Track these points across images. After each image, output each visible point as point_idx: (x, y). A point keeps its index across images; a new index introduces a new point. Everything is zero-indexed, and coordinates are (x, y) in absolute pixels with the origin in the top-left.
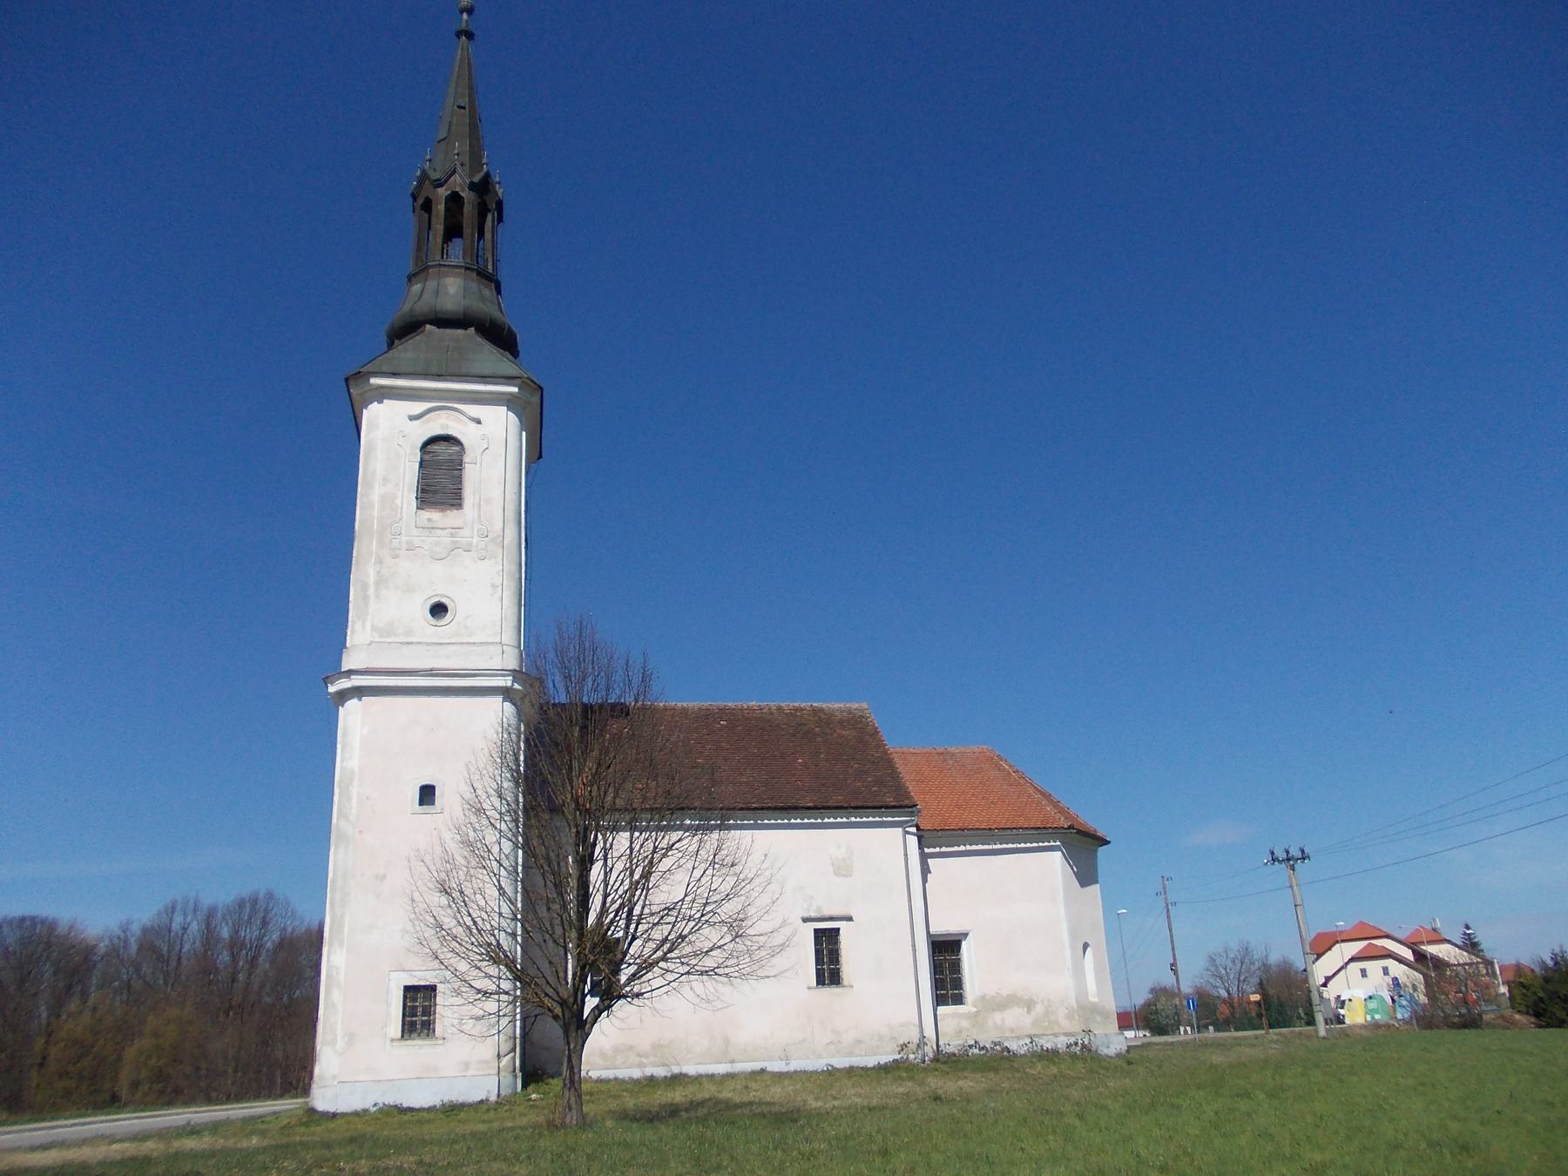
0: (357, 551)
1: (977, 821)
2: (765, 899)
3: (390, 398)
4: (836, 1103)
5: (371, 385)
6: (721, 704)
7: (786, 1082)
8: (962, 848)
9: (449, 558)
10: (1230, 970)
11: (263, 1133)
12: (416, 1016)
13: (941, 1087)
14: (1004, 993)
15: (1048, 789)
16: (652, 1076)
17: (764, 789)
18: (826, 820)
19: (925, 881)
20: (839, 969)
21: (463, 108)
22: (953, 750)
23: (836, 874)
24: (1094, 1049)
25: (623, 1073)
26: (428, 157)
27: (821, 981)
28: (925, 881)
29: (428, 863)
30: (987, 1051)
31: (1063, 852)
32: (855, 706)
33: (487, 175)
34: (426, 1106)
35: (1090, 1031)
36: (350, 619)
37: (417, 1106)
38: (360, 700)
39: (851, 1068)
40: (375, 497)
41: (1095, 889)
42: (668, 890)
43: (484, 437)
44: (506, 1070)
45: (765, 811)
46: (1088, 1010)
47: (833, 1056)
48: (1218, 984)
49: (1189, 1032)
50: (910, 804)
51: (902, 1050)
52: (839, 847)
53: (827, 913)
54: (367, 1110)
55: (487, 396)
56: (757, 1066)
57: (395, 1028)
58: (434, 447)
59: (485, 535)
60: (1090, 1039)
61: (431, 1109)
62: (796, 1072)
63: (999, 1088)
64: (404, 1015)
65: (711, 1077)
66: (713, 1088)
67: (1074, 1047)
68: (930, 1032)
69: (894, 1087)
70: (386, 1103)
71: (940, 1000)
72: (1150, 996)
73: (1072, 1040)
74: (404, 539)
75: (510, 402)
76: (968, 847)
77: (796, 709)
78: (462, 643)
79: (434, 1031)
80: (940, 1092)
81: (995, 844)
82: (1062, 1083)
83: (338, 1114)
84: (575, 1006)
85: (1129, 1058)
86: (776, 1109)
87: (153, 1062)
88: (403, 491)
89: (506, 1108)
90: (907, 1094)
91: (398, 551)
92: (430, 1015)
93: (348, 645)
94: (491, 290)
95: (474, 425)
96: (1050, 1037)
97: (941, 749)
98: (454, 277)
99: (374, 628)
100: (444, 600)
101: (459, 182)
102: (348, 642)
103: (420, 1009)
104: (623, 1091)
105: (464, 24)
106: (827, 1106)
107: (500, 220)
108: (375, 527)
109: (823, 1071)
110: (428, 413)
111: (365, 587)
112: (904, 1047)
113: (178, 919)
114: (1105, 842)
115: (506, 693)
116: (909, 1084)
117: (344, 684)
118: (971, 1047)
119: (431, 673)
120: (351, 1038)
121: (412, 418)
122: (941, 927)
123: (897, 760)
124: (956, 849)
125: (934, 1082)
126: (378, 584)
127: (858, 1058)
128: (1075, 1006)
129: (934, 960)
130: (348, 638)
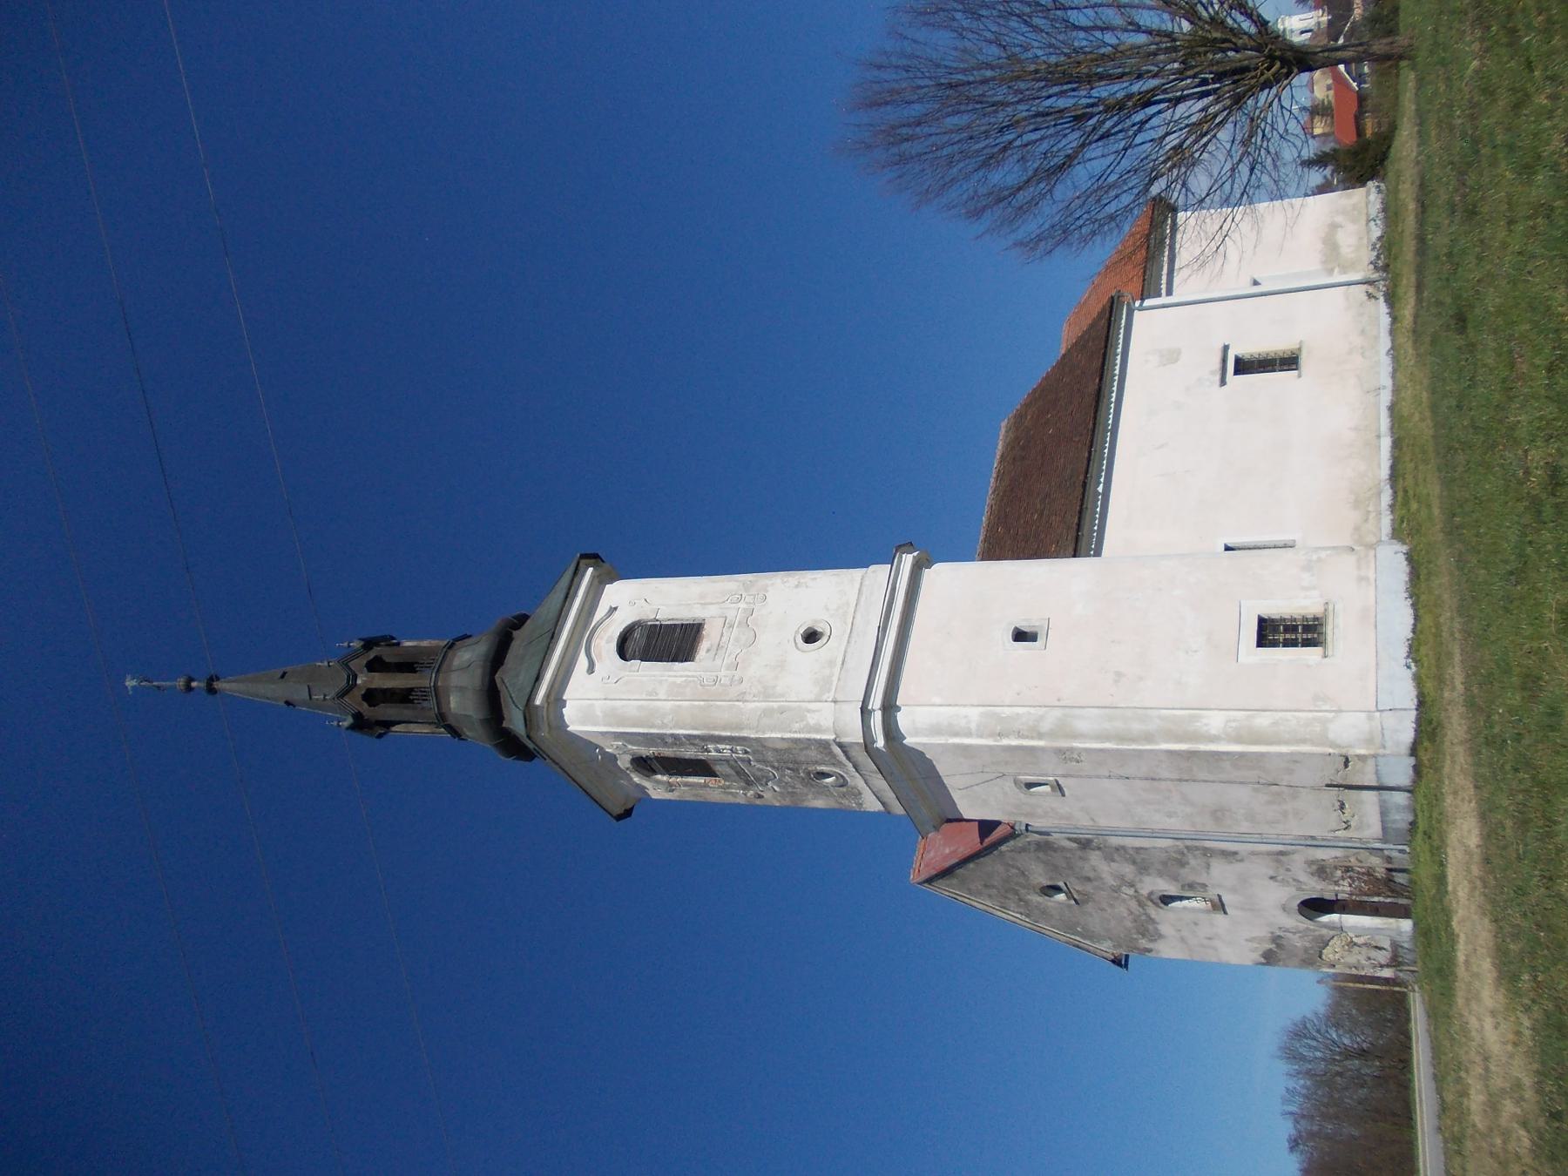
0: (724, 729)
18: (1117, 372)
23: (1177, 360)
34: (1412, 622)
38: (898, 709)
55: (590, 598)
58: (630, 647)
70: (1405, 655)
95: (616, 614)
103: (1288, 636)
119: (883, 629)
121: (591, 669)
127: (1382, 330)
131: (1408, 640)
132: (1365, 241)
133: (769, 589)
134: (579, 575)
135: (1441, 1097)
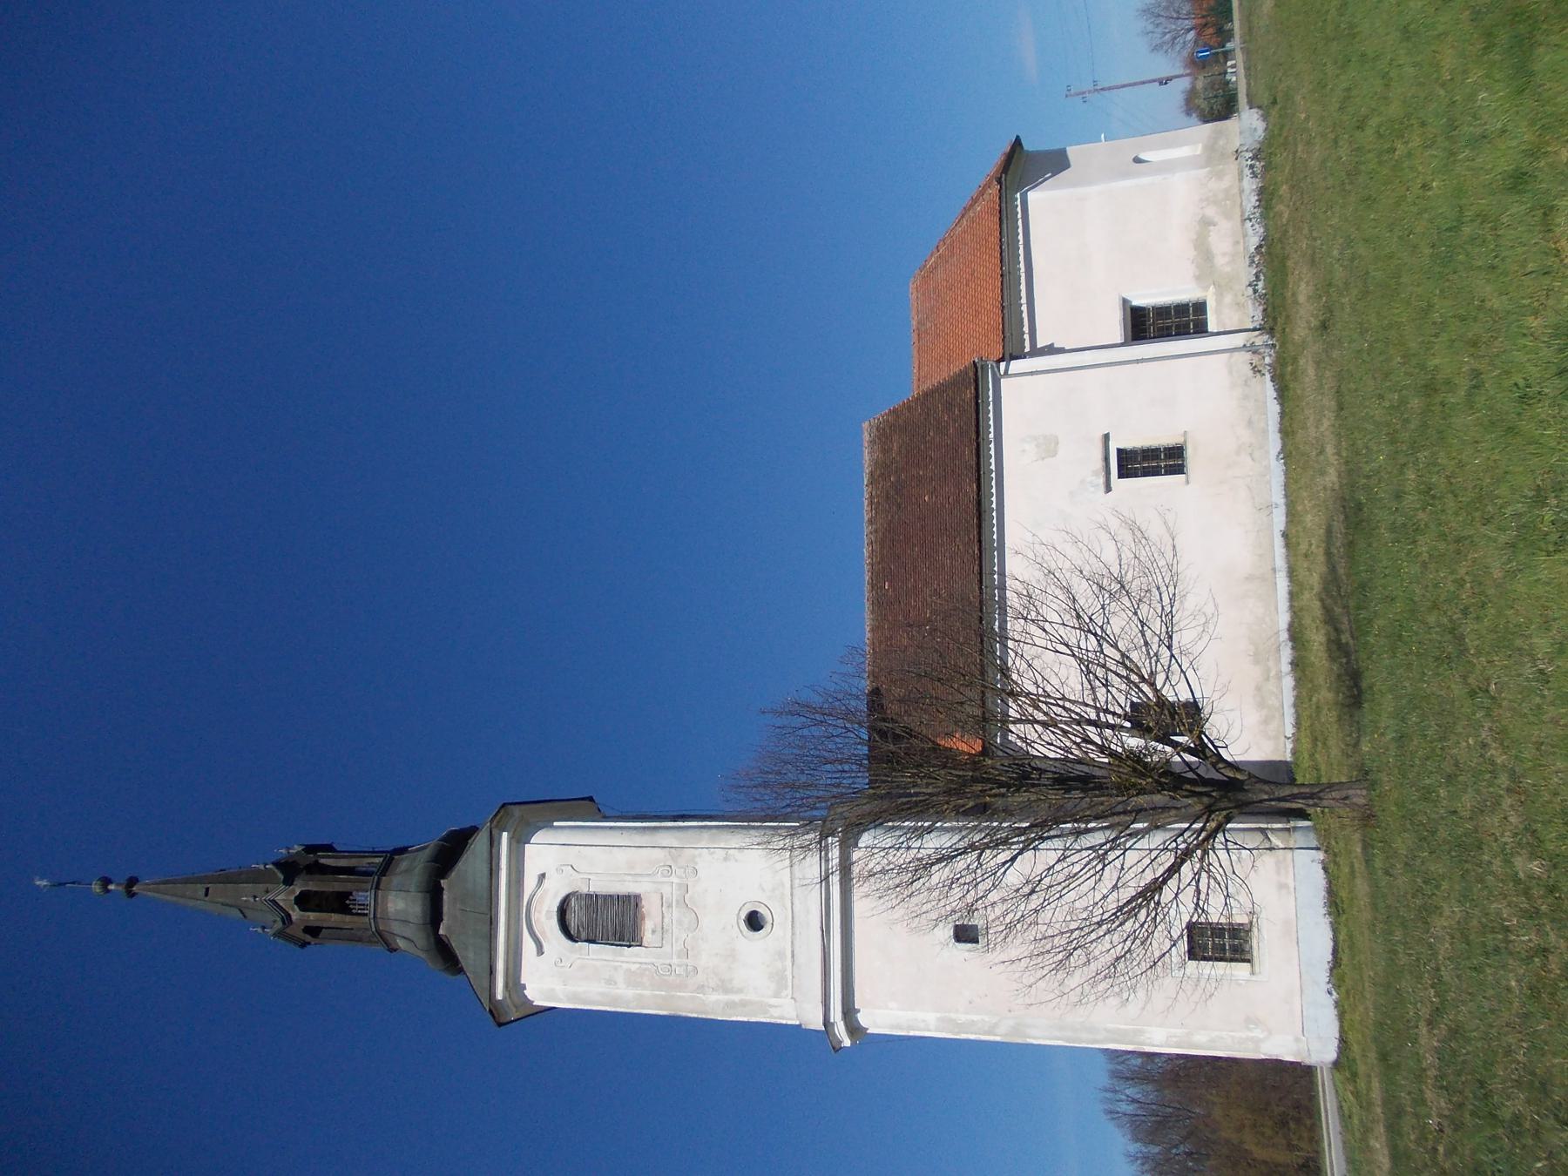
1: (993, 291)
2: (1071, 551)
3: (519, 977)
4: (1330, 450)
5: (504, 998)
6: (867, 587)
7: (1299, 508)
8: (1024, 308)
9: (695, 909)
10: (1166, 28)
11: (1367, 1130)
12: (1224, 944)
13: (1308, 322)
14: (1192, 253)
15: (959, 211)
16: (1291, 664)
17: (958, 540)
18: (993, 467)
19: (1062, 351)
20: (1165, 448)
21: (207, 889)
22: (914, 323)
23: (1054, 454)
24: (1258, 146)
25: (1288, 697)
26: (259, 930)
27: (1179, 469)
28: (1062, 351)
29: (1032, 980)
30: (1260, 272)
31: (1028, 190)
32: (866, 437)
33: (276, 864)
35: (1237, 151)
36: (768, 1020)
37: (1331, 944)
38: (859, 1011)
39: (1281, 431)
40: (630, 993)
41: (1072, 152)
42: (1065, 678)
43: (560, 870)
44: (1288, 841)
45: (983, 538)
46: (1212, 156)
47: (1267, 452)
48: (1181, 41)
49: (1234, 62)
50: (973, 369)
51: (1259, 371)
52: (1024, 451)
53: (1100, 464)
54: (1336, 1002)
56: (1279, 542)
57: (1240, 970)
58: (573, 922)
59: (669, 869)
60: (1247, 151)
61: (1335, 931)
62: (1286, 496)
63: (1310, 252)
64: (1221, 959)
65: (1293, 596)
66: (1307, 595)
67: (1255, 169)
68: (1239, 340)
69: (1307, 379)
71: (1201, 329)
72: (1194, 115)
73: (1247, 172)
74: (675, 961)
75: (519, 841)
76: (1024, 301)
77: (871, 503)
78: (792, 895)
79: (1242, 924)
80: (1314, 323)
81: (1020, 269)
82: (1302, 176)
83: (1340, 1036)
84: (1214, 794)
85: (1270, 105)
86: (1339, 527)
87: (1269, 1132)
88: (622, 962)
89: (1333, 843)
90: (1318, 363)
91: (690, 968)
92: (1224, 929)
93: (798, 1023)
94: (402, 859)
95: (546, 882)
96: (1243, 198)
97: (914, 337)
98: (387, 904)
99: (777, 995)
100: (743, 915)
101: (285, 896)
102: (793, 1022)
104: (1310, 700)
105: (120, 888)
106: (1336, 462)
107: (329, 848)
108: (663, 993)
109: (1285, 464)
110: (535, 936)
111: (730, 1005)
112: (1256, 370)
113: (1125, 1107)
114: (1018, 143)
115: (848, 845)
116: (1302, 362)
117: (840, 1030)
118: (1255, 291)
120: (1251, 1021)
121: (540, 951)
122: (1114, 329)
123: (927, 386)
124: (1025, 315)
125: (1301, 330)
126: (726, 991)
127: (1270, 423)
128: (1208, 169)
129: (1154, 338)
130: (789, 1022)
131: (1329, 962)
132: (1241, 247)
133: (697, 860)
134: (496, 843)
135: (1250, 22)
